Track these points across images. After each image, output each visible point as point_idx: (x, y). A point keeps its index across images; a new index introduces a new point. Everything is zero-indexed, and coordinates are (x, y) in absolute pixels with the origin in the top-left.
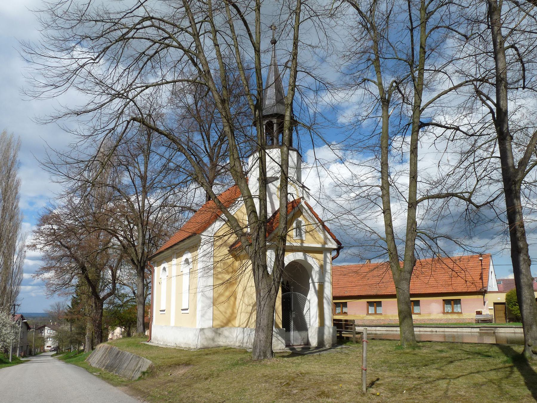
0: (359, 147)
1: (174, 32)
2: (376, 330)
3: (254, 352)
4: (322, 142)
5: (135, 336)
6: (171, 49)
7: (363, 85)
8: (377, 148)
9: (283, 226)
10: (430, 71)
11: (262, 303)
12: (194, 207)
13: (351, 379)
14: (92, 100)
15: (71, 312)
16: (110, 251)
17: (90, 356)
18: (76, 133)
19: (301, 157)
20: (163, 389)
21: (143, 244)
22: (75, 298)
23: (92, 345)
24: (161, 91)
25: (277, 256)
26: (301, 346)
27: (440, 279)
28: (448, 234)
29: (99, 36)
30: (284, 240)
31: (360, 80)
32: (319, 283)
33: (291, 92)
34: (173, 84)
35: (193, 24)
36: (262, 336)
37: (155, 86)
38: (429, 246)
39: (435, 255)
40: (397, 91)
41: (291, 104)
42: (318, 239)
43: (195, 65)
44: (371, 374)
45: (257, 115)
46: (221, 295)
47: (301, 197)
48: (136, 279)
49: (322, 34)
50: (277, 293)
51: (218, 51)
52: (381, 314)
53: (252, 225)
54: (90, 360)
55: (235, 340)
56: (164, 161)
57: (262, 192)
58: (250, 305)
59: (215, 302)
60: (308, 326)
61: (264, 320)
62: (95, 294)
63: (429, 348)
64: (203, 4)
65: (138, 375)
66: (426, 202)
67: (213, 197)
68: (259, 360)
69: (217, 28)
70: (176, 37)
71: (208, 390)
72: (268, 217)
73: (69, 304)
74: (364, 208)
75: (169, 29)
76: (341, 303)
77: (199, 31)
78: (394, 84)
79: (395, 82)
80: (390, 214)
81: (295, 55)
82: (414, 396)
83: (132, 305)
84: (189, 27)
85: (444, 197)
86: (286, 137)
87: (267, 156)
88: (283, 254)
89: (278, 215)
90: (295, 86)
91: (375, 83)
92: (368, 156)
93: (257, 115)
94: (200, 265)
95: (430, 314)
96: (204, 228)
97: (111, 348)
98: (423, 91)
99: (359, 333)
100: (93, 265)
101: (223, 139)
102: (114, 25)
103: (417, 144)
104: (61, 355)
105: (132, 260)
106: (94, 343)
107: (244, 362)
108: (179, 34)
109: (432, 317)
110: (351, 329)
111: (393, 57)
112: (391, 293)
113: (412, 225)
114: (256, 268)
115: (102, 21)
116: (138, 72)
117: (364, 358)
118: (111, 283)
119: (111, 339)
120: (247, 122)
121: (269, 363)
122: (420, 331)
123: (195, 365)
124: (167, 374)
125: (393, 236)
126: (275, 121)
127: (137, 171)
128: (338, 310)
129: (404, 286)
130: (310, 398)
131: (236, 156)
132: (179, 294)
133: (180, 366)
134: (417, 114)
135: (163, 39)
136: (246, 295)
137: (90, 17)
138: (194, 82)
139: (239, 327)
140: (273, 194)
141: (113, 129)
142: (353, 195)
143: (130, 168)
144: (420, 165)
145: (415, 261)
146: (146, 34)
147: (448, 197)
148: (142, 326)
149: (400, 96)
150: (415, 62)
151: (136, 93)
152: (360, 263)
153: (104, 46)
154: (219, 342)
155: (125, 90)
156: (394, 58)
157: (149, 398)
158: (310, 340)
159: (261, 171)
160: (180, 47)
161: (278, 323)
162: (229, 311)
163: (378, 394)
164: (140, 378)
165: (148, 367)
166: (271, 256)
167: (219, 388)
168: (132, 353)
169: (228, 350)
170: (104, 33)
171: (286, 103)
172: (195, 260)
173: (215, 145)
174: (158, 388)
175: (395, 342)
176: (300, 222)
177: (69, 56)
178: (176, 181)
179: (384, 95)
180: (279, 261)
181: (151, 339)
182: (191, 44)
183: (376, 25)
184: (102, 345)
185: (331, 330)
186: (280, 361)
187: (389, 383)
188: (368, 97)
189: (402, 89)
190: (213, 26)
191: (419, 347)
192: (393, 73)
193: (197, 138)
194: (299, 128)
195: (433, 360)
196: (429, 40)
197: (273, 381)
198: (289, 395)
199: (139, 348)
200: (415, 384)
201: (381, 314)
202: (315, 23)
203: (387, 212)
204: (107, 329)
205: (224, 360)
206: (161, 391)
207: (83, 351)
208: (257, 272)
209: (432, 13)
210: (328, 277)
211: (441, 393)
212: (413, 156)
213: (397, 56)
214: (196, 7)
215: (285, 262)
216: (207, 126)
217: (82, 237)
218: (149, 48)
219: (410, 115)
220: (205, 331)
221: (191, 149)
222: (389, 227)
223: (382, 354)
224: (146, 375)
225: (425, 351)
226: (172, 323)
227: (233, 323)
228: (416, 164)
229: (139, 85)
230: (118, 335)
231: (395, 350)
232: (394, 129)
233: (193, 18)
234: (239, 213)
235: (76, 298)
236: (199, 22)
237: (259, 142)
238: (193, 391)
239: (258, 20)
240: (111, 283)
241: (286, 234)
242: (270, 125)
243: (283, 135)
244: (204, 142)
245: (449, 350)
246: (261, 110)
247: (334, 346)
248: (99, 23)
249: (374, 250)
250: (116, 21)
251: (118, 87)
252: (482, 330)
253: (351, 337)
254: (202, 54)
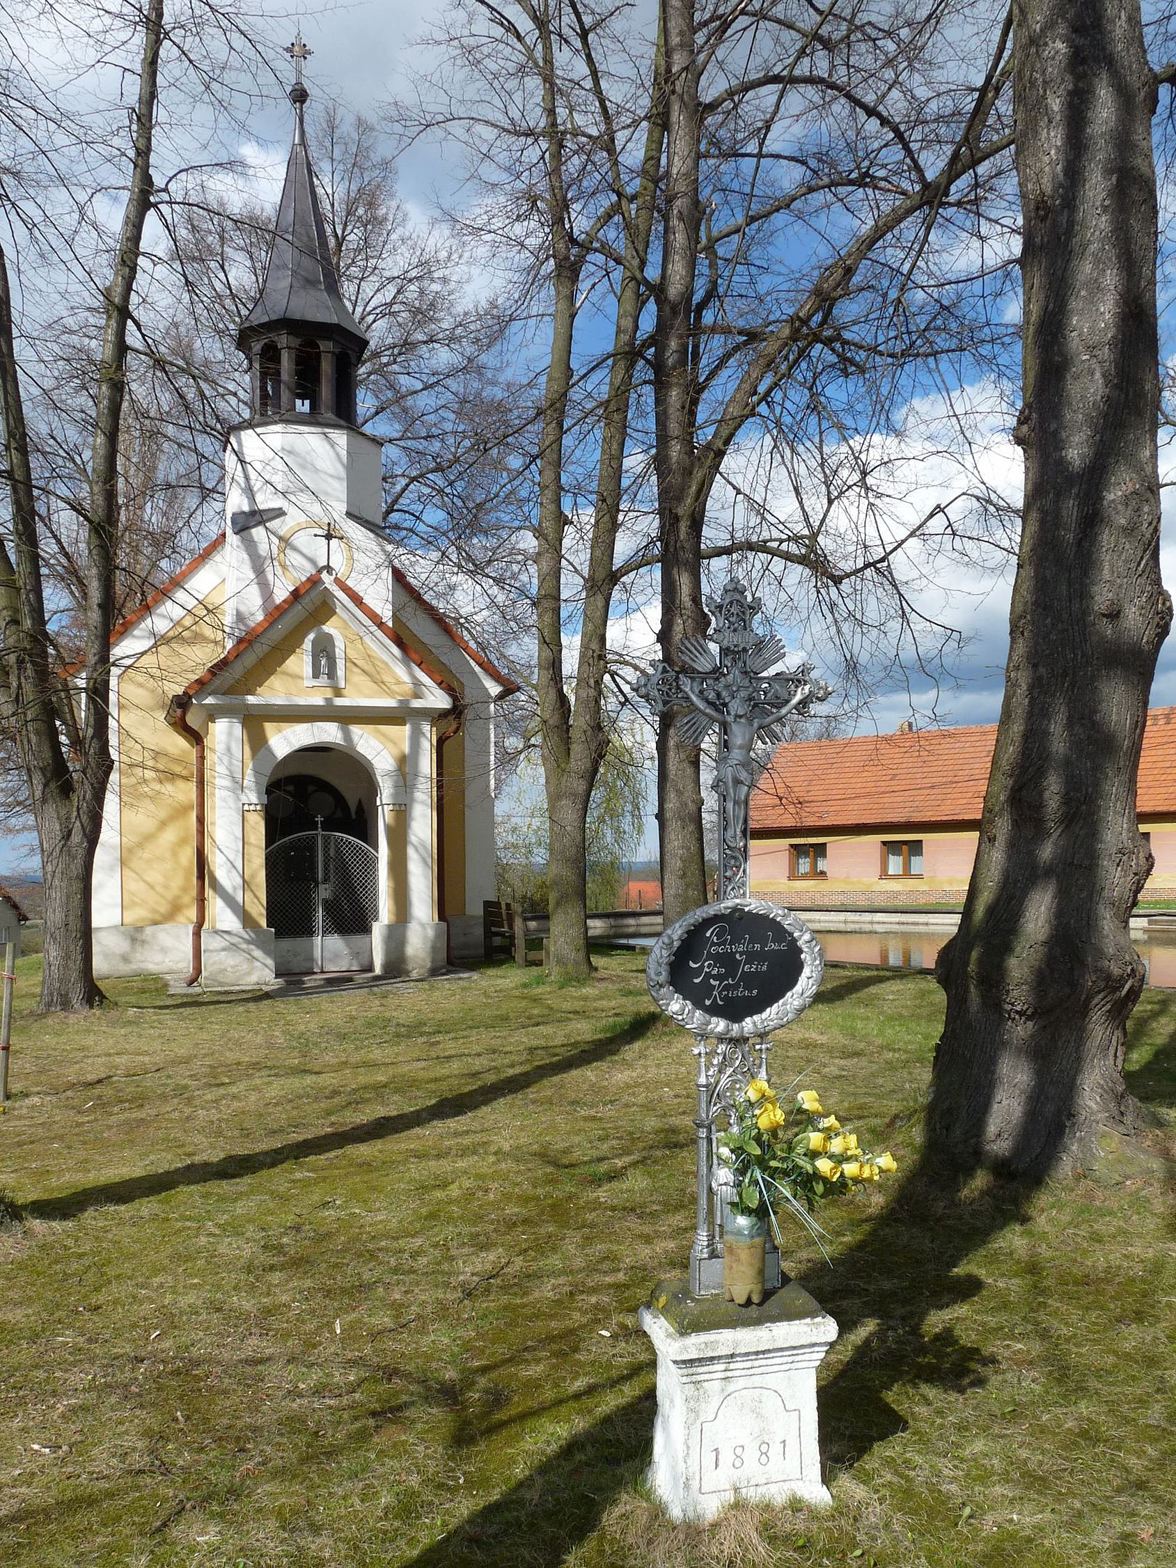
2: (872, 923)
47: (323, 568)
52: (920, 877)
76: (812, 845)
126: (283, 340)
185: (431, 933)
252: (1156, 922)
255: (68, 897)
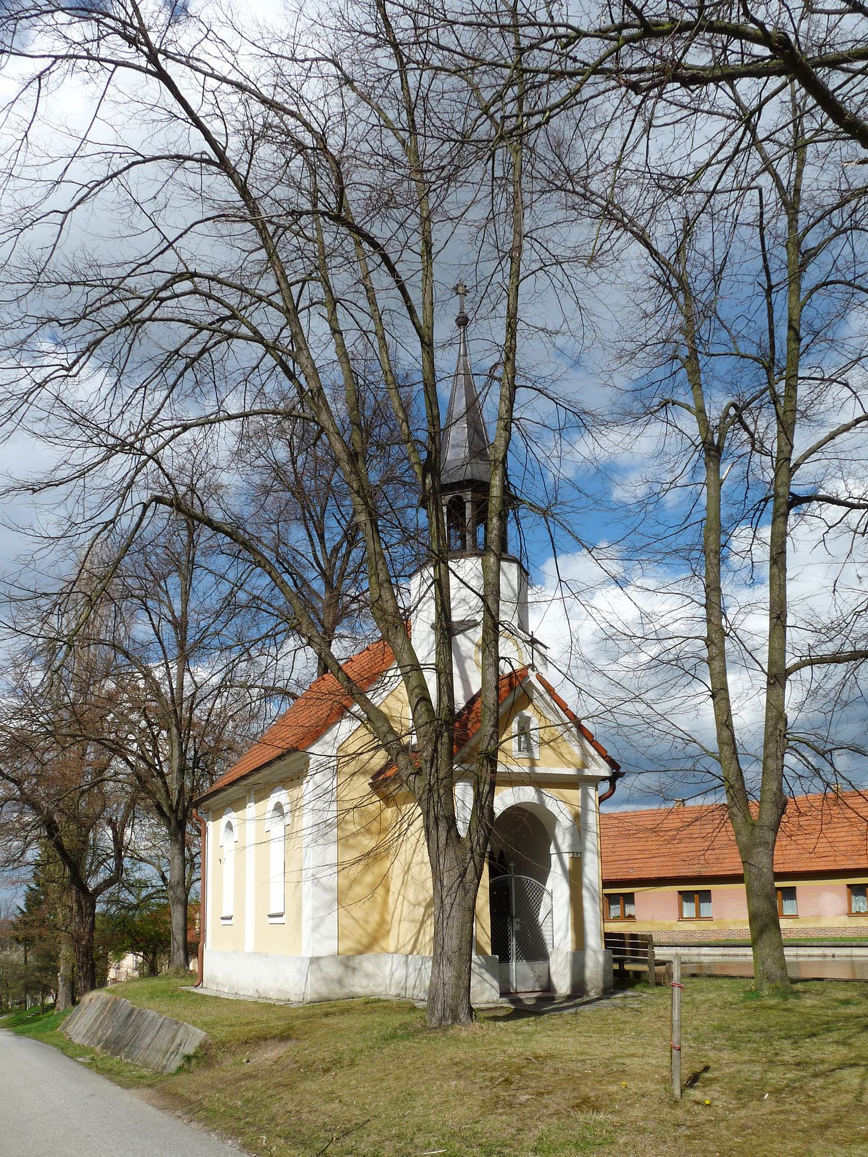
0: (657, 552)
1: (243, 305)
2: (699, 955)
3: (430, 1009)
4: (574, 542)
5: (167, 974)
6: (237, 343)
7: (662, 414)
8: (696, 554)
9: (490, 730)
10: (810, 381)
11: (448, 901)
12: (293, 689)
13: (648, 1067)
14: (65, 458)
15: (26, 923)
16: (109, 786)
17: (68, 1019)
18: (31, 532)
19: (527, 574)
20: (232, 1095)
21: (182, 770)
22: (32, 889)
23: (72, 993)
24: (216, 437)
25: (478, 797)
26: (535, 995)
27: (840, 839)
28: (857, 742)
29: (77, 316)
30: (491, 759)
31: (656, 401)
32: (571, 855)
33: (504, 434)
34: (241, 419)
35: (284, 284)
36: (449, 974)
37: (203, 424)
38: (815, 769)
39: (828, 790)
40: (737, 425)
41: (504, 460)
42: (568, 757)
43: (291, 376)
44: (691, 1055)
45: (428, 487)
46: (355, 881)
47: (530, 665)
48: (166, 848)
49: (569, 304)
50: (479, 879)
51: (341, 346)
52: (710, 919)
53: (421, 730)
54: (69, 1029)
55: (388, 982)
56: (225, 588)
57: (442, 657)
58: (419, 904)
59: (341, 897)
60: (550, 950)
61: (451, 938)
62: (78, 882)
63: (818, 994)
64: (305, 241)
65: (177, 1062)
66: (806, 671)
67: (335, 668)
68: (441, 1027)
69: (337, 295)
70: (247, 315)
71: (331, 1097)
72: (457, 711)
73: (21, 903)
74: (666, 687)
75: (233, 298)
77: (298, 301)
78: (732, 411)
79: (734, 405)
80: (728, 700)
81: (510, 351)
82: (787, 1107)
83: (159, 905)
84: (274, 294)
85: (847, 660)
86: (494, 534)
87: (451, 575)
88: (492, 792)
89: (478, 705)
90: (512, 420)
91: (688, 408)
92: (677, 572)
93: (428, 487)
94: (307, 820)
95: (819, 917)
96: (316, 733)
97: (116, 1002)
98: (796, 426)
99: (663, 963)
100: (74, 818)
101: (353, 538)
102: (111, 292)
103: (784, 542)
104: (5, 1017)
105: (159, 807)
106: (77, 989)
107: (408, 1032)
108: (252, 308)
109: (824, 924)
110: (645, 954)
111: (728, 351)
112: (733, 872)
113: (777, 723)
114: (431, 824)
115: (84, 284)
116: (165, 393)
117: (676, 1024)
118: (112, 857)
119: (115, 980)
120: (406, 499)
121: (464, 1034)
122: (797, 956)
123: (302, 1041)
124: (241, 1061)
125: (735, 748)
126: (468, 496)
127: (165, 611)
128: (615, 910)
129: (760, 858)
130: (557, 1113)
131: (382, 576)
132: (263, 883)
133: (269, 1042)
134: (783, 478)
135: (218, 321)
136: (410, 883)
137: (57, 277)
138: (287, 415)
139: (396, 952)
140: (466, 658)
141: (112, 521)
142: (644, 658)
143: (150, 603)
144: (792, 590)
145: (786, 803)
146: (182, 310)
147: (855, 660)
148: (182, 952)
149: (745, 436)
150: (778, 361)
151: (161, 441)
152: (663, 807)
153: (90, 338)
154: (352, 986)
155: (137, 434)
156: (732, 354)
157: (202, 1114)
158: (554, 979)
159: (439, 609)
160: (258, 338)
161: (483, 944)
162: (375, 918)
163: (707, 1102)
164: (180, 1069)
165: (197, 1044)
166: (464, 795)
167: (354, 1091)
168: (161, 1013)
169: (372, 1004)
170: (89, 309)
171: (492, 458)
172: (296, 808)
173: (336, 550)
174: (220, 1091)
175: (743, 982)
176: (528, 720)
177: (12, 362)
178: (254, 634)
179: (709, 435)
180: (482, 808)
181: (202, 980)
182: (281, 330)
183: (690, 280)
184: (94, 994)
185: (601, 959)
186: (487, 1029)
187: (732, 1077)
188: (673, 440)
189: (749, 421)
190: (329, 290)
191: (796, 994)
192: (730, 386)
193: (297, 535)
194: (521, 513)
195: (827, 1024)
196: (808, 313)
197: (474, 1074)
198: (511, 1105)
199: (177, 1002)
200: (790, 1079)
201: (710, 919)
202: (555, 281)
203: (720, 694)
204: (104, 957)
205: (365, 1029)
206: (228, 1099)
207: (53, 1006)
208: (433, 832)
209: (812, 254)
210: (592, 842)
211: (848, 1098)
212: (776, 570)
213: (737, 349)
214: (291, 248)
215: (495, 809)
216: (318, 509)
217: (47, 756)
218: (187, 342)
219: (769, 480)
220: (323, 963)
221: (285, 560)
222: (725, 729)
223: (716, 1009)
224: (194, 1061)
225: (809, 1001)
226: (249, 946)
227: (383, 943)
228: (783, 588)
229: (168, 424)
230: (130, 971)
231: (743, 1001)
232: (734, 511)
233: (283, 273)
234: (391, 702)
235: (36, 891)
236: (297, 282)
237: (434, 547)
238: (298, 1097)
239: (428, 275)
240: (112, 857)
241: (497, 749)
242: (457, 507)
243: (486, 529)
244: (313, 545)
245: (862, 999)
246: (436, 474)
247: (607, 992)
248: (77, 289)
249: (692, 780)
250: (115, 283)
251: (121, 429)
253: (644, 972)
254: (305, 352)
255: (462, 926)
